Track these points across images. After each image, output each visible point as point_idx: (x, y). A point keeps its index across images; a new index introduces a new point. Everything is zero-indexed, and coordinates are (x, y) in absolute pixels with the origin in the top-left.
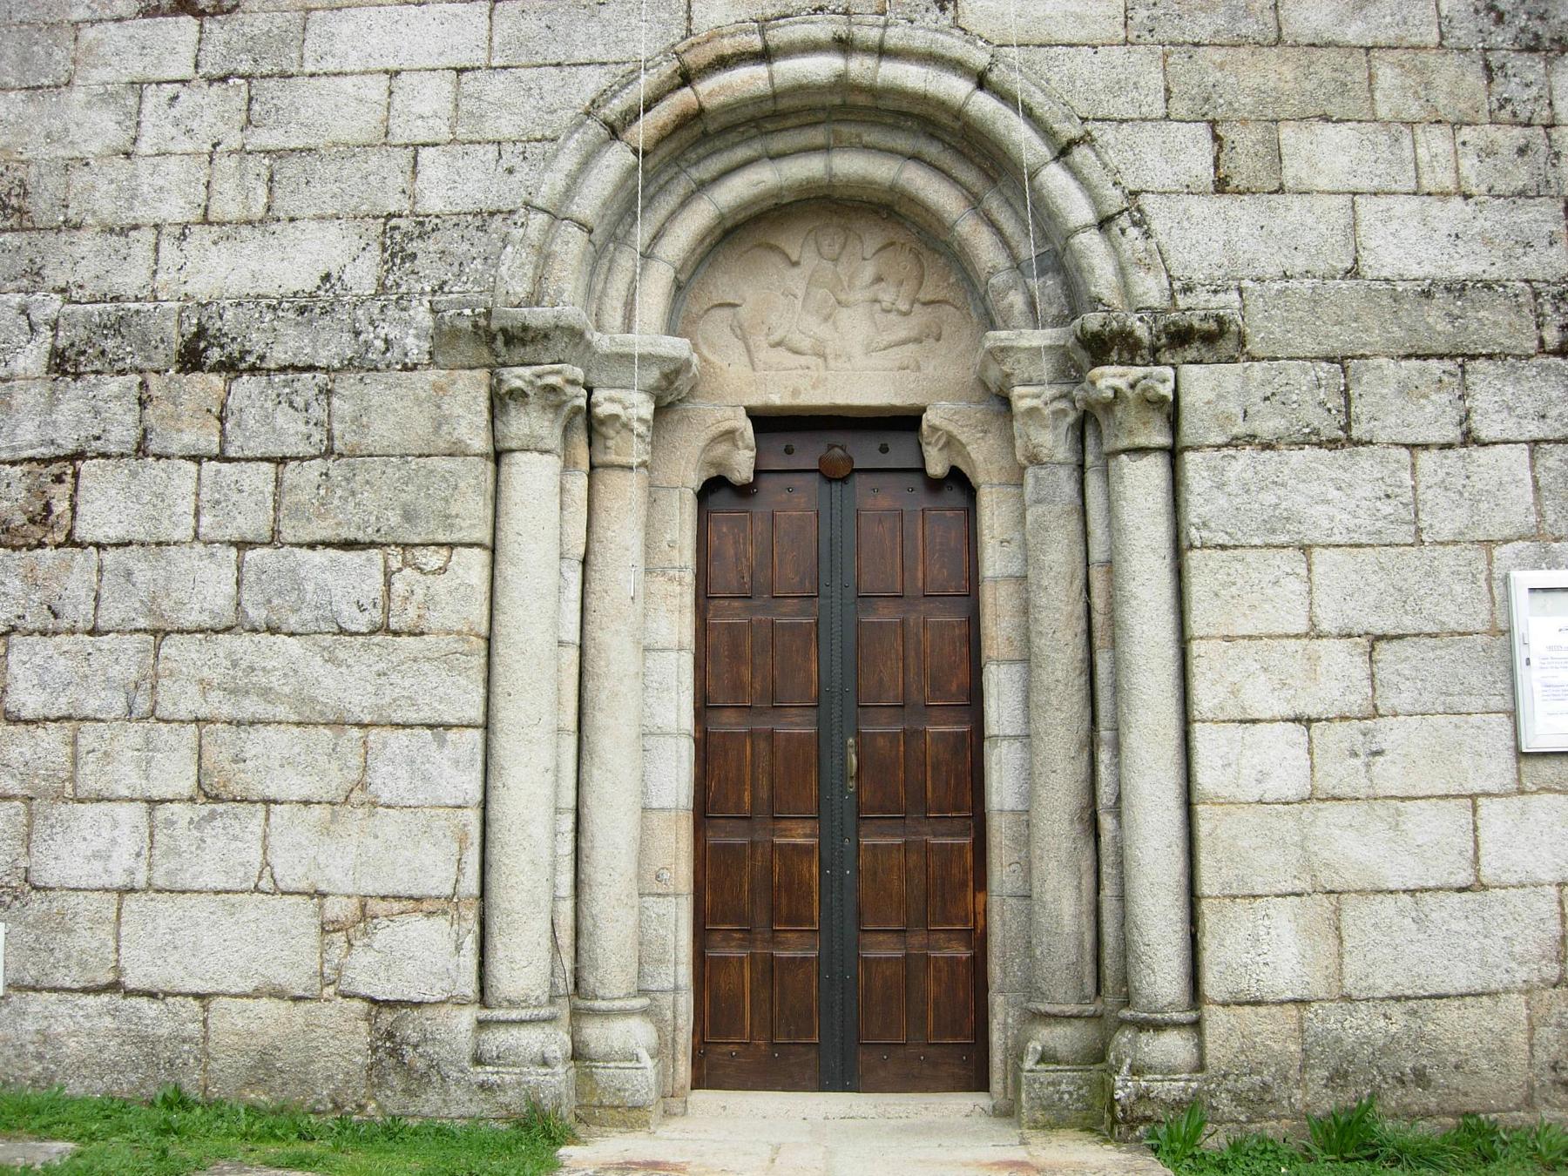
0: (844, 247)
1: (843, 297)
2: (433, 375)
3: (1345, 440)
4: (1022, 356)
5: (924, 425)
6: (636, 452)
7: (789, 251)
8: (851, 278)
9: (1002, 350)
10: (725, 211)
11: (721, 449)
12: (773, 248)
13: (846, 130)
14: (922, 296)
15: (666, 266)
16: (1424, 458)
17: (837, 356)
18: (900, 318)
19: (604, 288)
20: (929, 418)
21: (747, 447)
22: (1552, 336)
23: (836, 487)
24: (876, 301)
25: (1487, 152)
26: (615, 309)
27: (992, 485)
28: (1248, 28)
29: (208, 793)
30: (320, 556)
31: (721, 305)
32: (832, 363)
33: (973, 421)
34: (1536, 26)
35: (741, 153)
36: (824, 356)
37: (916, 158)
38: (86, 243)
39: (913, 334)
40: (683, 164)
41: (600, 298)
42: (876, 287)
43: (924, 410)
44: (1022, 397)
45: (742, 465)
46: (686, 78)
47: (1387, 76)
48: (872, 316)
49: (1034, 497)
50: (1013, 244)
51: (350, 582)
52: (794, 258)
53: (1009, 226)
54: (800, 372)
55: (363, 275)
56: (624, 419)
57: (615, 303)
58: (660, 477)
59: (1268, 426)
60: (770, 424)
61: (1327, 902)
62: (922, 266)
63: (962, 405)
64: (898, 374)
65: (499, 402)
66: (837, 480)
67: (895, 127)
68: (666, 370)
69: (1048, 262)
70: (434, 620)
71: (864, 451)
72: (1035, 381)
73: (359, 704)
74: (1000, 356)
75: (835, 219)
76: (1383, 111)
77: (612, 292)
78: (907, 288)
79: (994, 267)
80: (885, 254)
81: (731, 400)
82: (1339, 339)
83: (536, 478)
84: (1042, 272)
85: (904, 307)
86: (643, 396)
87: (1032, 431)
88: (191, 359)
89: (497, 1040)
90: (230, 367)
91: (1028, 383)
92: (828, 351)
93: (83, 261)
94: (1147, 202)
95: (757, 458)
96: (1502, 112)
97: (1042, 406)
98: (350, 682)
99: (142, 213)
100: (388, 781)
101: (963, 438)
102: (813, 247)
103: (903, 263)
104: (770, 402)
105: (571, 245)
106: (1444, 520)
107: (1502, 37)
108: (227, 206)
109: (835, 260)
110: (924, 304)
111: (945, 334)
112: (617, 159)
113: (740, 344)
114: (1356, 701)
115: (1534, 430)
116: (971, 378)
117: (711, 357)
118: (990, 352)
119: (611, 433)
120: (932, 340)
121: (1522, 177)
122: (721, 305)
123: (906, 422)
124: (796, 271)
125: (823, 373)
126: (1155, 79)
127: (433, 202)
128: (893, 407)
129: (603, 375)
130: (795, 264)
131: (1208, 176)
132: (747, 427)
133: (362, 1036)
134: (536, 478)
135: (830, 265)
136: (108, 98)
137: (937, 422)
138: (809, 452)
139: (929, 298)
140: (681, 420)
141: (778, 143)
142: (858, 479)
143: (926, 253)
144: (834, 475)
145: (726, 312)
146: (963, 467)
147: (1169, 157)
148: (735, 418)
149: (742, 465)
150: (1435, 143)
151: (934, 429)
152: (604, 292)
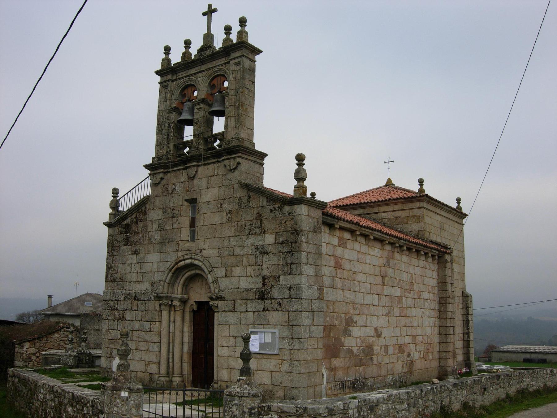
2: (154, 301)
3: (234, 311)
16: (242, 313)
22: (257, 297)
25: (254, 270)
28: (231, 253)
29: (137, 349)
30: (145, 323)
34: (262, 250)
38: (128, 283)
46: (177, 263)
47: (245, 259)
51: (147, 325)
55: (150, 288)
59: (226, 309)
61: (230, 370)
65: (160, 305)
70: (155, 330)
73: (148, 340)
76: (244, 265)
82: (234, 297)
83: (165, 313)
88: (135, 299)
89: (160, 378)
90: (138, 300)
93: (127, 286)
94: (219, 279)
96: (257, 264)
98: (147, 338)
99: (132, 280)
100: (151, 349)
105: (166, 285)
106: (243, 322)
107: (258, 252)
108: (139, 280)
112: (170, 274)
114: (233, 345)
115: (254, 310)
121: (258, 273)
126: (220, 261)
127: (156, 280)
131: (225, 275)
133: (148, 377)
134: (165, 313)
136: (129, 265)
147: (221, 272)
150: (249, 269)
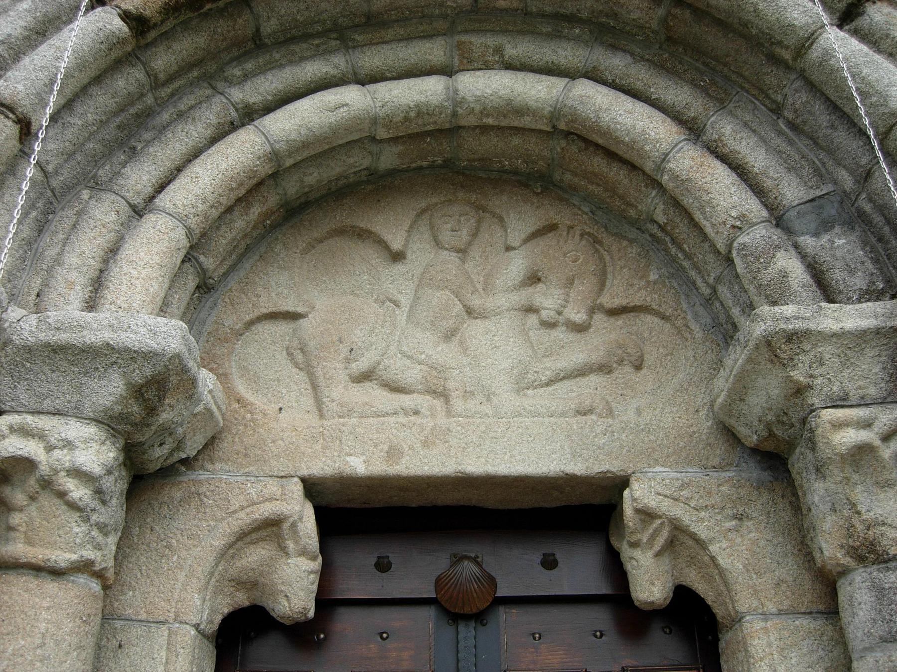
0: (475, 234)
1: (476, 302)
4: (826, 350)
5: (628, 510)
6: (66, 539)
7: (387, 237)
8: (488, 276)
9: (792, 337)
10: (281, 147)
11: (256, 555)
12: (364, 235)
13: (478, 42)
14: (607, 301)
15: (171, 222)
17: (468, 394)
18: (572, 336)
19: (61, 254)
20: (639, 494)
21: (303, 552)
23: (467, 631)
24: (530, 310)
26: (71, 285)
27: (766, 616)
31: (273, 316)
32: (458, 404)
33: (716, 499)
35: (313, 69)
36: (443, 395)
37: (595, 76)
39: (597, 356)
40: (220, 85)
41: (50, 270)
42: (531, 290)
43: (623, 482)
44: (838, 425)
45: (294, 584)
48: (524, 332)
49: (880, 630)
50: (768, 183)
52: (396, 245)
53: (757, 159)
54: (402, 419)
56: (44, 469)
57: (73, 275)
58: (133, 601)
60: (353, 515)
62: (601, 258)
63: (693, 473)
64: (575, 422)
66: (467, 618)
67: (556, 36)
68: (138, 378)
69: (831, 210)
71: (516, 569)
72: (853, 400)
74: (785, 351)
75: (461, 195)
77: (72, 259)
78: (583, 287)
79: (742, 217)
80: (542, 243)
81: (280, 466)
84: (825, 226)
85: (579, 317)
86: (91, 430)
87: (860, 495)
91: (841, 402)
92: (451, 385)
95: (326, 576)
97: (877, 443)
101: (702, 531)
102: (427, 235)
103: (568, 253)
104: (347, 471)
109: (462, 252)
110: (614, 313)
111: (649, 360)
113: (302, 376)
116: (705, 425)
117: (250, 396)
118: (768, 342)
119: (18, 497)
120: (628, 369)
122: (273, 316)
123: (585, 512)
124: (399, 268)
125: (442, 420)
128: (570, 481)
129: (21, 389)
130: (397, 257)
132: (309, 525)
135: (454, 257)
137: (651, 502)
138: (417, 571)
139: (617, 302)
140: (185, 501)
141: (371, 59)
142: (505, 616)
143: (607, 240)
144: (463, 610)
145: (282, 328)
146: (701, 588)
148: (283, 498)
149: (294, 584)
151: (646, 515)
152: (58, 260)
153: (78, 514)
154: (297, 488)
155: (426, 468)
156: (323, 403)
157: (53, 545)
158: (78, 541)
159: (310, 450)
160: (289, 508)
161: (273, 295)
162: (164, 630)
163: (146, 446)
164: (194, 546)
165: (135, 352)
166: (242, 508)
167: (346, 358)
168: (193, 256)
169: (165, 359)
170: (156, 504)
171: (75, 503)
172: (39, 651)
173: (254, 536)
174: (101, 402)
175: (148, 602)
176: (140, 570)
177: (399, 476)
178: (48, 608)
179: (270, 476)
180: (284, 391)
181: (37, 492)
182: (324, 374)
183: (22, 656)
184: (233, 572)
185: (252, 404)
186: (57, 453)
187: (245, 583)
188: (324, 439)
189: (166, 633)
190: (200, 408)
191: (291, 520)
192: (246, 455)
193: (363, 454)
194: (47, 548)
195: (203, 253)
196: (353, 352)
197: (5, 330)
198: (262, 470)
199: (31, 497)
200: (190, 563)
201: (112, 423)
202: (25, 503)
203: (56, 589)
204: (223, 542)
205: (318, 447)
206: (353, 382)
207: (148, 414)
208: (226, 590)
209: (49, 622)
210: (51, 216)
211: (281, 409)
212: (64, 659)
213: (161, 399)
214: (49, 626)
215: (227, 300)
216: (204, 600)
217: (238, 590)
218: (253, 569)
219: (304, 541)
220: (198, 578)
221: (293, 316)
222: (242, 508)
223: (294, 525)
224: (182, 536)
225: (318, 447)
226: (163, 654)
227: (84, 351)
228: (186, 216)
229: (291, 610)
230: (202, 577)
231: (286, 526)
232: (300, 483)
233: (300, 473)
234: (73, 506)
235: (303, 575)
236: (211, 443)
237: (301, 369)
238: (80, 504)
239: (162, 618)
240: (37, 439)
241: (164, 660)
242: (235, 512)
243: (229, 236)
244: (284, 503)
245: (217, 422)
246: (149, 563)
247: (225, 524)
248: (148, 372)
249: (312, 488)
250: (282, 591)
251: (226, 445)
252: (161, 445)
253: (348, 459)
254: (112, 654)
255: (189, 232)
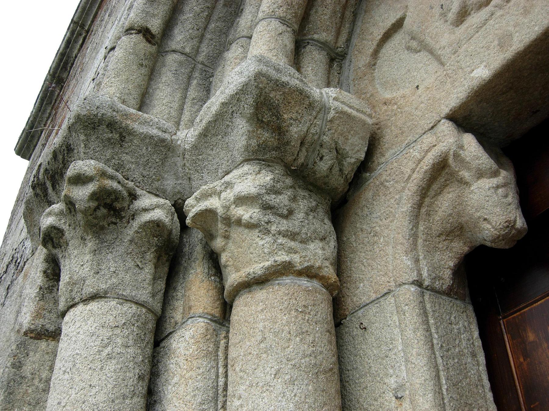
11: (445, 203)
31: (387, 36)
68: (249, 111)
122: (387, 36)
140: (376, 195)
145: (398, 39)
153: (257, 231)
154: (447, 127)
155: (536, 29)
156: (439, 56)
157: (249, 263)
158: (266, 250)
159: (443, 93)
160: (445, 144)
161: (381, 24)
162: (390, 299)
163: (310, 166)
164: (391, 222)
165: (236, 94)
166: (413, 171)
167: (441, 14)
168: (309, 39)
169: (252, 82)
170: (359, 211)
171: (249, 222)
172: (262, 345)
173: (435, 186)
174: (240, 145)
175: (373, 284)
176: (363, 264)
177: (518, 53)
178: (262, 310)
179: (424, 134)
180: (415, 74)
181: (226, 231)
182: (431, 37)
183: (250, 353)
184: (436, 228)
185: (393, 99)
186: (223, 195)
187: (451, 232)
188: (450, 77)
189: (392, 300)
190: (332, 114)
191: (451, 153)
192: (402, 133)
193: (481, 62)
194: (247, 267)
195: (315, 33)
196: (444, 7)
197: (180, 145)
198: (417, 133)
199: (225, 237)
200: (392, 236)
201: (258, 156)
202: (223, 243)
203: (265, 294)
204: (410, 205)
205: (448, 86)
206: (457, 26)
207: (279, 134)
208: (440, 246)
209: (264, 320)
210: (211, 79)
211: (417, 87)
212: (287, 345)
213: (278, 116)
214: (266, 323)
215: (356, 52)
216: (417, 261)
217: (452, 241)
218: (450, 215)
219: (475, 164)
220: (401, 244)
221: (398, 25)
222: (413, 171)
223: (456, 156)
224: (381, 220)
225: (448, 86)
226: (395, 318)
227: (216, 121)
228: (273, 12)
229: (496, 229)
230: (405, 241)
231: (451, 161)
232: (447, 121)
233: (442, 116)
234: (251, 226)
235: (489, 193)
236: (373, 144)
237: (420, 51)
238: (252, 221)
239: (385, 291)
240: (213, 196)
241: (397, 323)
242: (410, 177)
243: (328, 12)
244: (441, 144)
245: (364, 123)
246: (367, 255)
247: (406, 191)
248: (251, 101)
249: (462, 119)
250: (479, 218)
251: (388, 137)
252: (321, 159)
253: (472, 75)
254: (362, 338)
255: (283, 21)
